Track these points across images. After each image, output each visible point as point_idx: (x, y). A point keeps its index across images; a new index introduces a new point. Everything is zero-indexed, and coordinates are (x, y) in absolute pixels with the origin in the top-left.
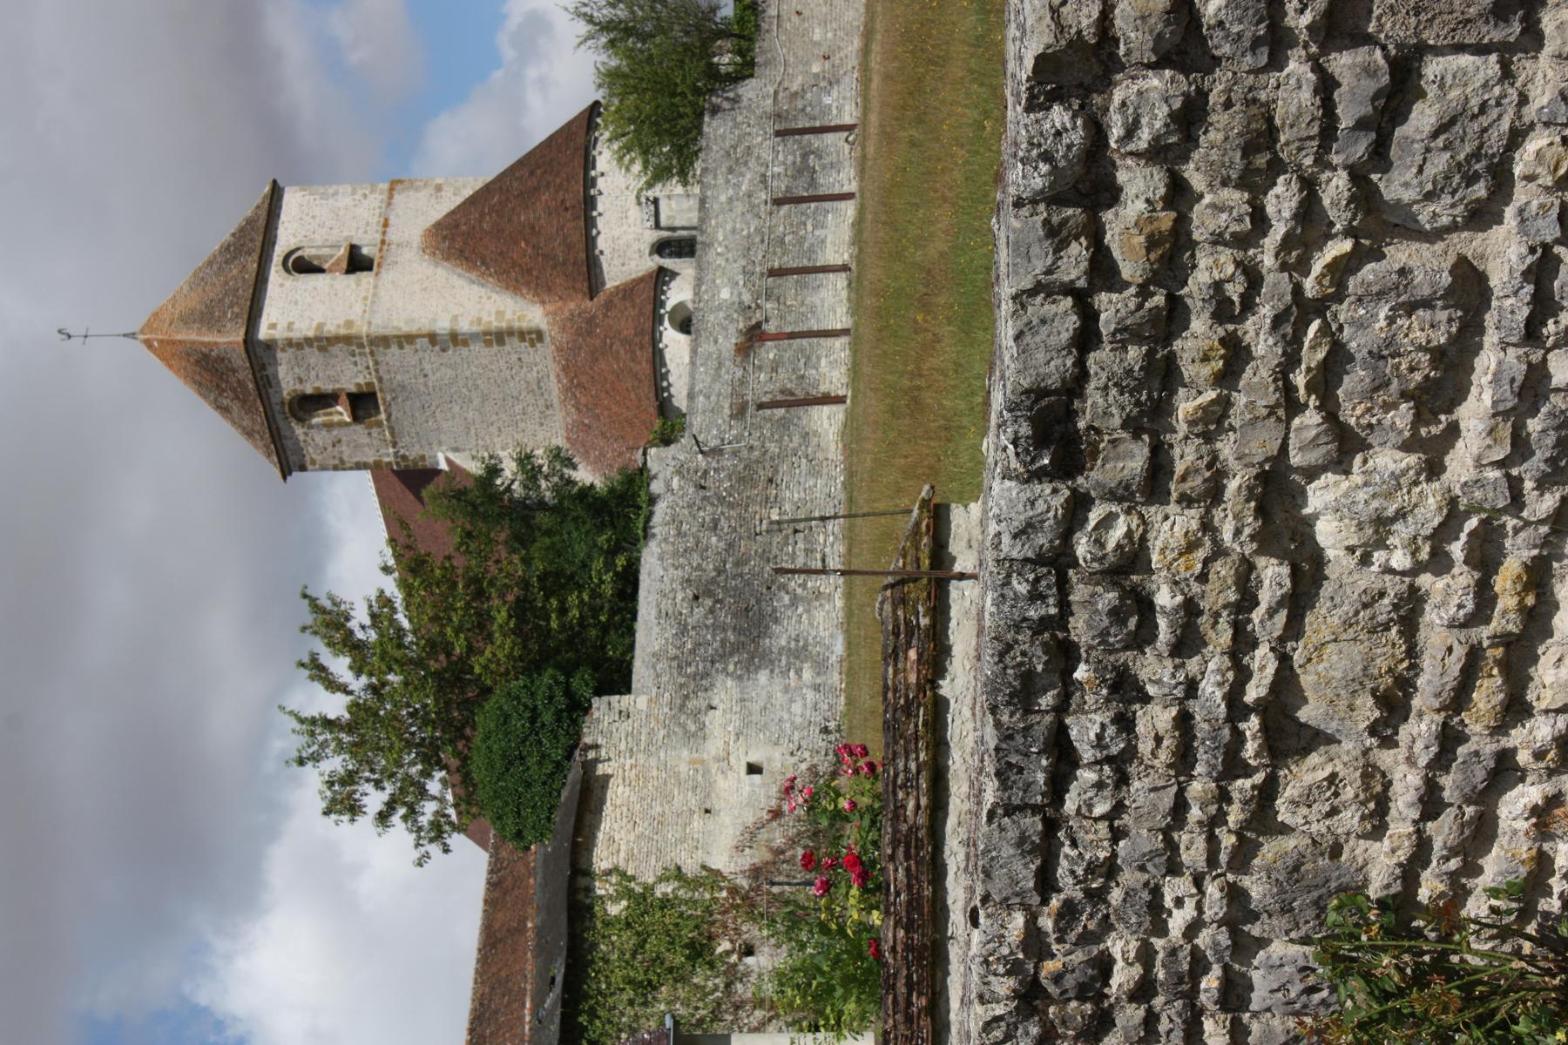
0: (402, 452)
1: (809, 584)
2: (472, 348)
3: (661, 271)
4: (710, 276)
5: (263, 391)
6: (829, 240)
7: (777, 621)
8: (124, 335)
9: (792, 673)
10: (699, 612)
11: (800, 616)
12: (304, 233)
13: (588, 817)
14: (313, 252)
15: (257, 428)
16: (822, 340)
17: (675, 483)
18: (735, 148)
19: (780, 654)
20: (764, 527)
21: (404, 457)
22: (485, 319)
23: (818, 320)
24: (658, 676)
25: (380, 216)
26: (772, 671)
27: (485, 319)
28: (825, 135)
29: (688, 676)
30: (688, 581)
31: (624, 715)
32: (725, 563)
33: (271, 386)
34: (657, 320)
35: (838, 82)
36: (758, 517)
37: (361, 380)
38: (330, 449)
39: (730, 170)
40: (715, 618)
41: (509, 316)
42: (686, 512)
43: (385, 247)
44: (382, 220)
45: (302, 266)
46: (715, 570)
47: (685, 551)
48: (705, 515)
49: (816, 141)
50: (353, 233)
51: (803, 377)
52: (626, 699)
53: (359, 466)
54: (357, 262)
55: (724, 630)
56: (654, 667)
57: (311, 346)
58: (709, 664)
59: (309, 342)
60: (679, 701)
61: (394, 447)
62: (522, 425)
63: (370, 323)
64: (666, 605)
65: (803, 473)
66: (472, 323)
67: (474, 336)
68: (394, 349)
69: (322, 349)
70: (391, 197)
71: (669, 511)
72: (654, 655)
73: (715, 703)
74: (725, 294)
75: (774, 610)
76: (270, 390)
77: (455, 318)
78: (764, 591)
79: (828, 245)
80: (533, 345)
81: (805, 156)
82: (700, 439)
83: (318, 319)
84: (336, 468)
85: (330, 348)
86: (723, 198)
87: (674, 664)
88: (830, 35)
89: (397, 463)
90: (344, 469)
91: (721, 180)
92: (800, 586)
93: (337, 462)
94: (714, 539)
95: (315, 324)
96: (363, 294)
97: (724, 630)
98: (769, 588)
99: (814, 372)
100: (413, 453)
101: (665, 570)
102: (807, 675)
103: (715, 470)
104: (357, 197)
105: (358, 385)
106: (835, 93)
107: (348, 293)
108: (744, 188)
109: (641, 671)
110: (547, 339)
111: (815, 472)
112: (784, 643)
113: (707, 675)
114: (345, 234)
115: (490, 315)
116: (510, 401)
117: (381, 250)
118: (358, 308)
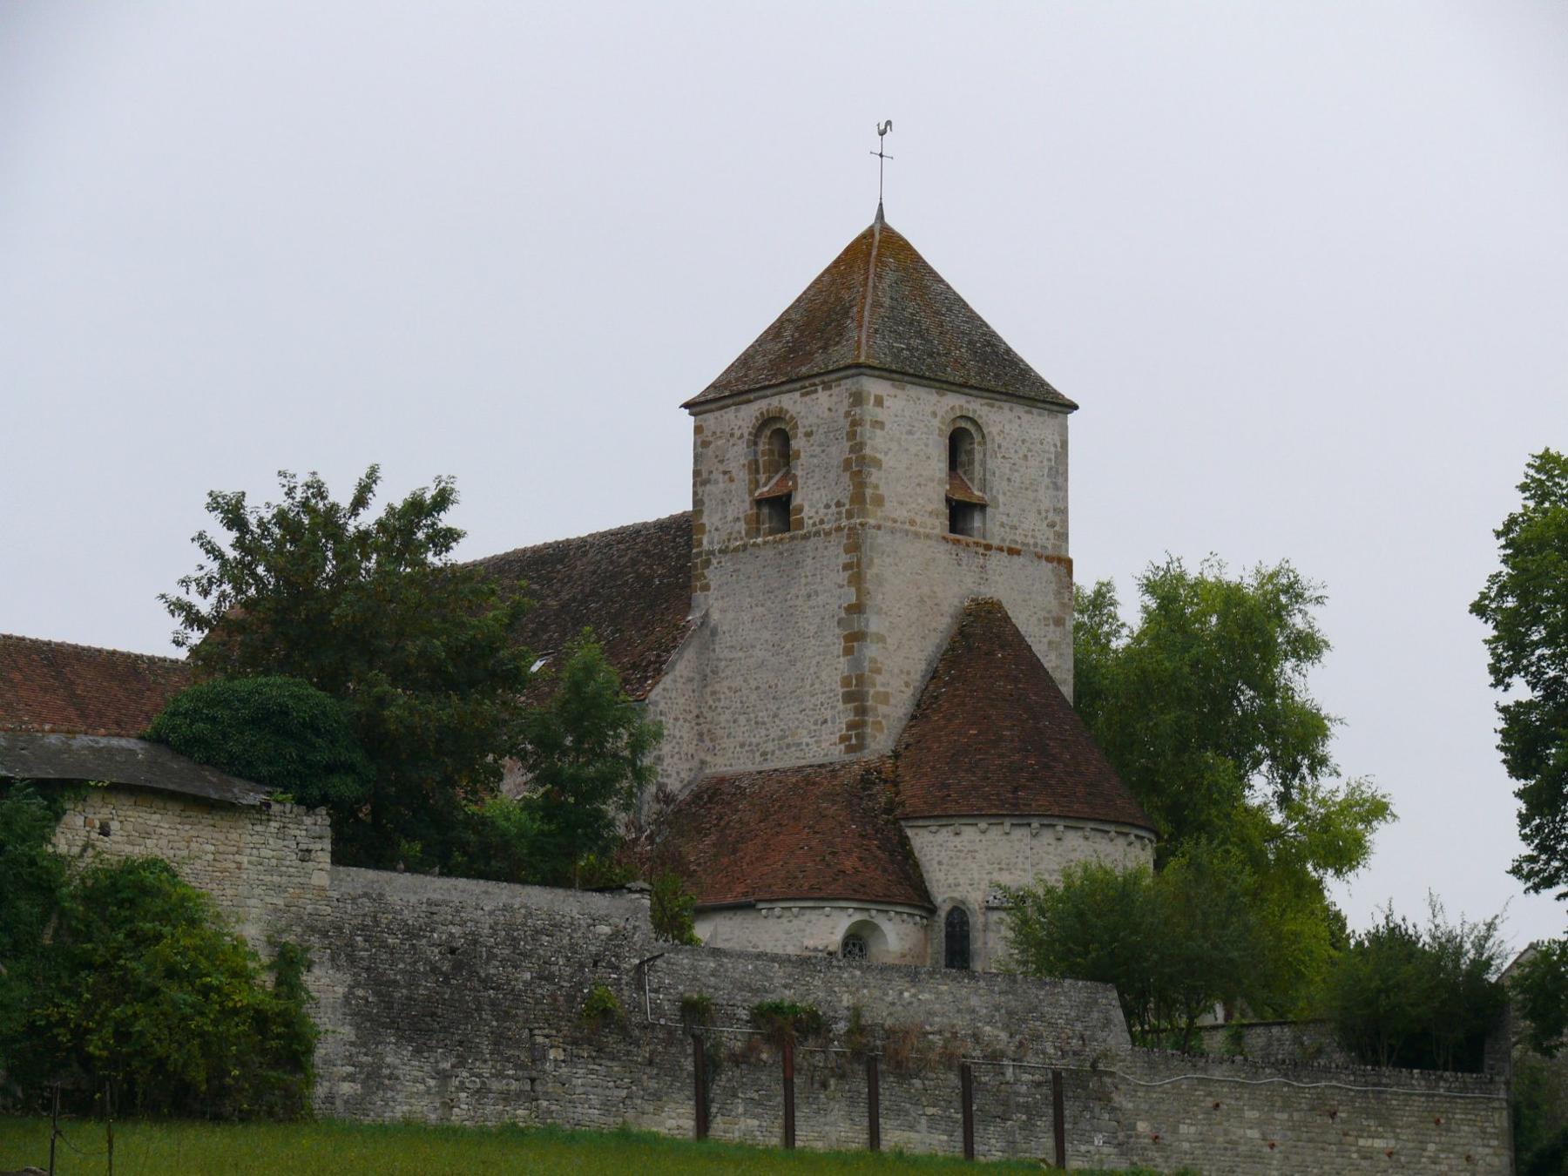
0: (715, 561)
2: (842, 659)
3: (931, 910)
4: (872, 982)
5: (798, 385)
6: (913, 1135)
7: (418, 1052)
8: (881, 204)
9: (350, 1069)
10: (434, 954)
11: (423, 1082)
12: (1004, 444)
14: (978, 457)
16: (780, 1121)
17: (605, 929)
18: (1041, 1017)
20: (540, 1039)
21: (707, 563)
22: (879, 679)
23: (807, 1118)
24: (354, 900)
25: (1023, 544)
26: (352, 1044)
27: (879, 679)
28: (1051, 1134)
30: (475, 942)
31: (305, 855)
32: (497, 989)
33: (803, 395)
35: (1122, 1154)
36: (554, 1032)
37: (807, 512)
38: (721, 468)
39: (1010, 1013)
40: (425, 973)
41: (882, 709)
42: (566, 941)
43: (981, 550)
44: (1019, 547)
45: (960, 444)
46: (487, 975)
47: (514, 939)
48: (560, 965)
49: (1044, 1123)
50: (1002, 509)
51: (735, 1096)
52: (326, 858)
53: (698, 502)
54: (960, 513)
55: (409, 986)
56: (366, 895)
57: (852, 451)
58: (366, 963)
59: (858, 448)
60: (320, 925)
61: (721, 551)
62: (742, 720)
63: (879, 527)
64: (445, 913)
65: (607, 1092)
66: (874, 661)
67: (856, 664)
68: (844, 558)
69: (847, 464)
70: (1049, 559)
71: (568, 919)
72: (381, 895)
75: (431, 1049)
76: (797, 394)
77: (881, 639)
78: (457, 1038)
79: (906, 1134)
80: (843, 739)
81: (1026, 1108)
82: (659, 962)
83: (888, 461)
84: (696, 473)
85: (848, 474)
86: (974, 1001)
87: (368, 921)
88: (1186, 1146)
89: (699, 554)
90: (695, 485)
91: (998, 999)
92: (462, 1083)
93: (705, 475)
94: (528, 976)
95: (879, 456)
96: (918, 520)
97: (409, 986)
98: (461, 1043)
99: (741, 1110)
100: (713, 576)
101: (491, 913)
102: (346, 1088)
103: (619, 979)
104: (1051, 515)
105: (800, 509)
106: (1106, 1150)
107: (920, 501)
108: (988, 1028)
109: (363, 878)
110: (853, 757)
111: (607, 1106)
112: (388, 1060)
113: (352, 960)
114: (1001, 499)
115: (883, 685)
116: (773, 707)
117: (977, 544)
118: (902, 514)
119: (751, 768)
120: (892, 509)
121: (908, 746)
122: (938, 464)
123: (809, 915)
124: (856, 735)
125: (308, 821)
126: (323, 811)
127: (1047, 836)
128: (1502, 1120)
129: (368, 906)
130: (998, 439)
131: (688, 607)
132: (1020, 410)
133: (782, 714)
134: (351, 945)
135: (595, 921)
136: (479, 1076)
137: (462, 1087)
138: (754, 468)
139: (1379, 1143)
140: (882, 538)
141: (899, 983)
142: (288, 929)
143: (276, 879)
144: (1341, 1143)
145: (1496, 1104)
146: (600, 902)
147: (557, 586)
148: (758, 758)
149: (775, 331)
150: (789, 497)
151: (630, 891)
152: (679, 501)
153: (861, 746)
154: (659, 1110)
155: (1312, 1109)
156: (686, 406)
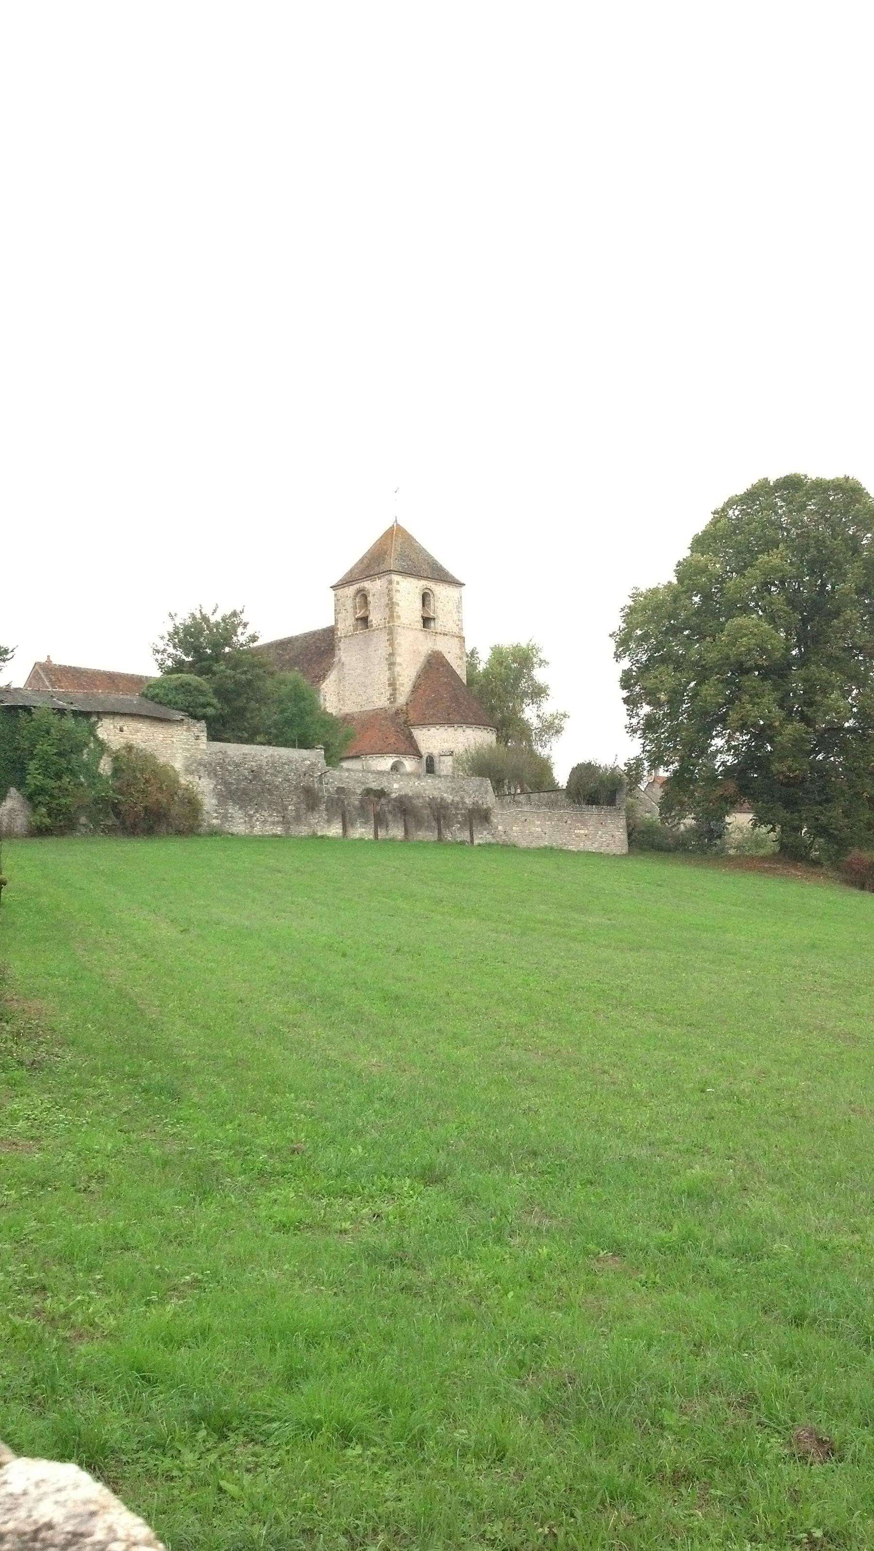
1: (258, 823)
3: (421, 757)
7: (240, 808)
9: (216, 815)
10: (246, 772)
13: (148, 721)
14: (432, 602)
15: (353, 575)
18: (464, 791)
19: (225, 809)
22: (400, 678)
27: (400, 678)
29: (215, 766)
30: (261, 768)
31: (197, 738)
34: (397, 752)
37: (374, 622)
39: (453, 789)
41: (402, 689)
42: (294, 767)
45: (425, 597)
52: (204, 739)
53: (336, 620)
54: (426, 621)
59: (391, 599)
66: (399, 672)
67: (393, 673)
70: (457, 637)
73: (202, 780)
74: (396, 786)
77: (401, 665)
80: (388, 699)
82: (328, 773)
94: (280, 780)
100: (342, 645)
101: (266, 757)
105: (372, 621)
109: (218, 746)
113: (216, 775)
114: (440, 616)
119: (357, 710)
120: (403, 620)
121: (411, 701)
122: (419, 604)
123: (380, 759)
124: (393, 698)
125: (198, 725)
126: (203, 722)
127: (460, 730)
128: (623, 822)
129: (221, 756)
130: (439, 596)
131: (334, 656)
132: (446, 586)
133: (367, 691)
134: (215, 770)
135: (305, 760)
136: (263, 816)
137: (257, 820)
138: (355, 608)
139: (582, 832)
140: (400, 630)
141: (413, 779)
142: (191, 764)
143: (187, 746)
144: (569, 832)
145: (621, 817)
146: (305, 753)
147: (288, 651)
148: (359, 707)
149: (362, 561)
150: (368, 617)
151: (317, 749)
152: (328, 622)
153: (395, 701)
154: (329, 826)
155: (559, 820)
156: (331, 587)
